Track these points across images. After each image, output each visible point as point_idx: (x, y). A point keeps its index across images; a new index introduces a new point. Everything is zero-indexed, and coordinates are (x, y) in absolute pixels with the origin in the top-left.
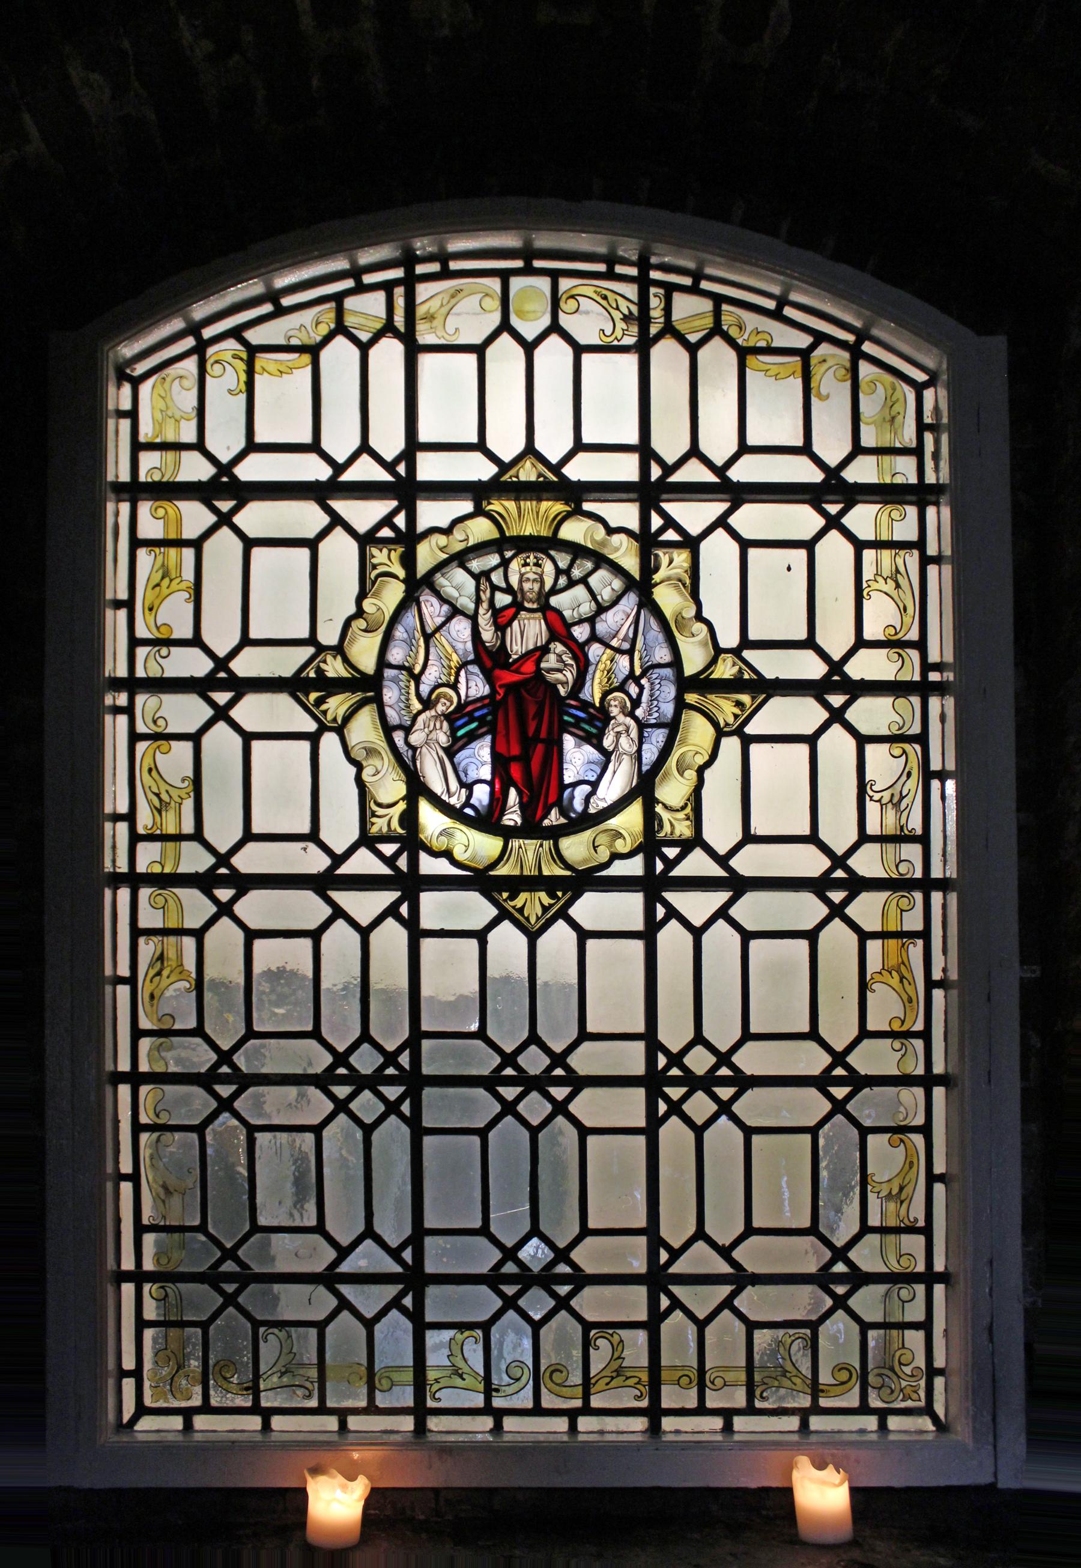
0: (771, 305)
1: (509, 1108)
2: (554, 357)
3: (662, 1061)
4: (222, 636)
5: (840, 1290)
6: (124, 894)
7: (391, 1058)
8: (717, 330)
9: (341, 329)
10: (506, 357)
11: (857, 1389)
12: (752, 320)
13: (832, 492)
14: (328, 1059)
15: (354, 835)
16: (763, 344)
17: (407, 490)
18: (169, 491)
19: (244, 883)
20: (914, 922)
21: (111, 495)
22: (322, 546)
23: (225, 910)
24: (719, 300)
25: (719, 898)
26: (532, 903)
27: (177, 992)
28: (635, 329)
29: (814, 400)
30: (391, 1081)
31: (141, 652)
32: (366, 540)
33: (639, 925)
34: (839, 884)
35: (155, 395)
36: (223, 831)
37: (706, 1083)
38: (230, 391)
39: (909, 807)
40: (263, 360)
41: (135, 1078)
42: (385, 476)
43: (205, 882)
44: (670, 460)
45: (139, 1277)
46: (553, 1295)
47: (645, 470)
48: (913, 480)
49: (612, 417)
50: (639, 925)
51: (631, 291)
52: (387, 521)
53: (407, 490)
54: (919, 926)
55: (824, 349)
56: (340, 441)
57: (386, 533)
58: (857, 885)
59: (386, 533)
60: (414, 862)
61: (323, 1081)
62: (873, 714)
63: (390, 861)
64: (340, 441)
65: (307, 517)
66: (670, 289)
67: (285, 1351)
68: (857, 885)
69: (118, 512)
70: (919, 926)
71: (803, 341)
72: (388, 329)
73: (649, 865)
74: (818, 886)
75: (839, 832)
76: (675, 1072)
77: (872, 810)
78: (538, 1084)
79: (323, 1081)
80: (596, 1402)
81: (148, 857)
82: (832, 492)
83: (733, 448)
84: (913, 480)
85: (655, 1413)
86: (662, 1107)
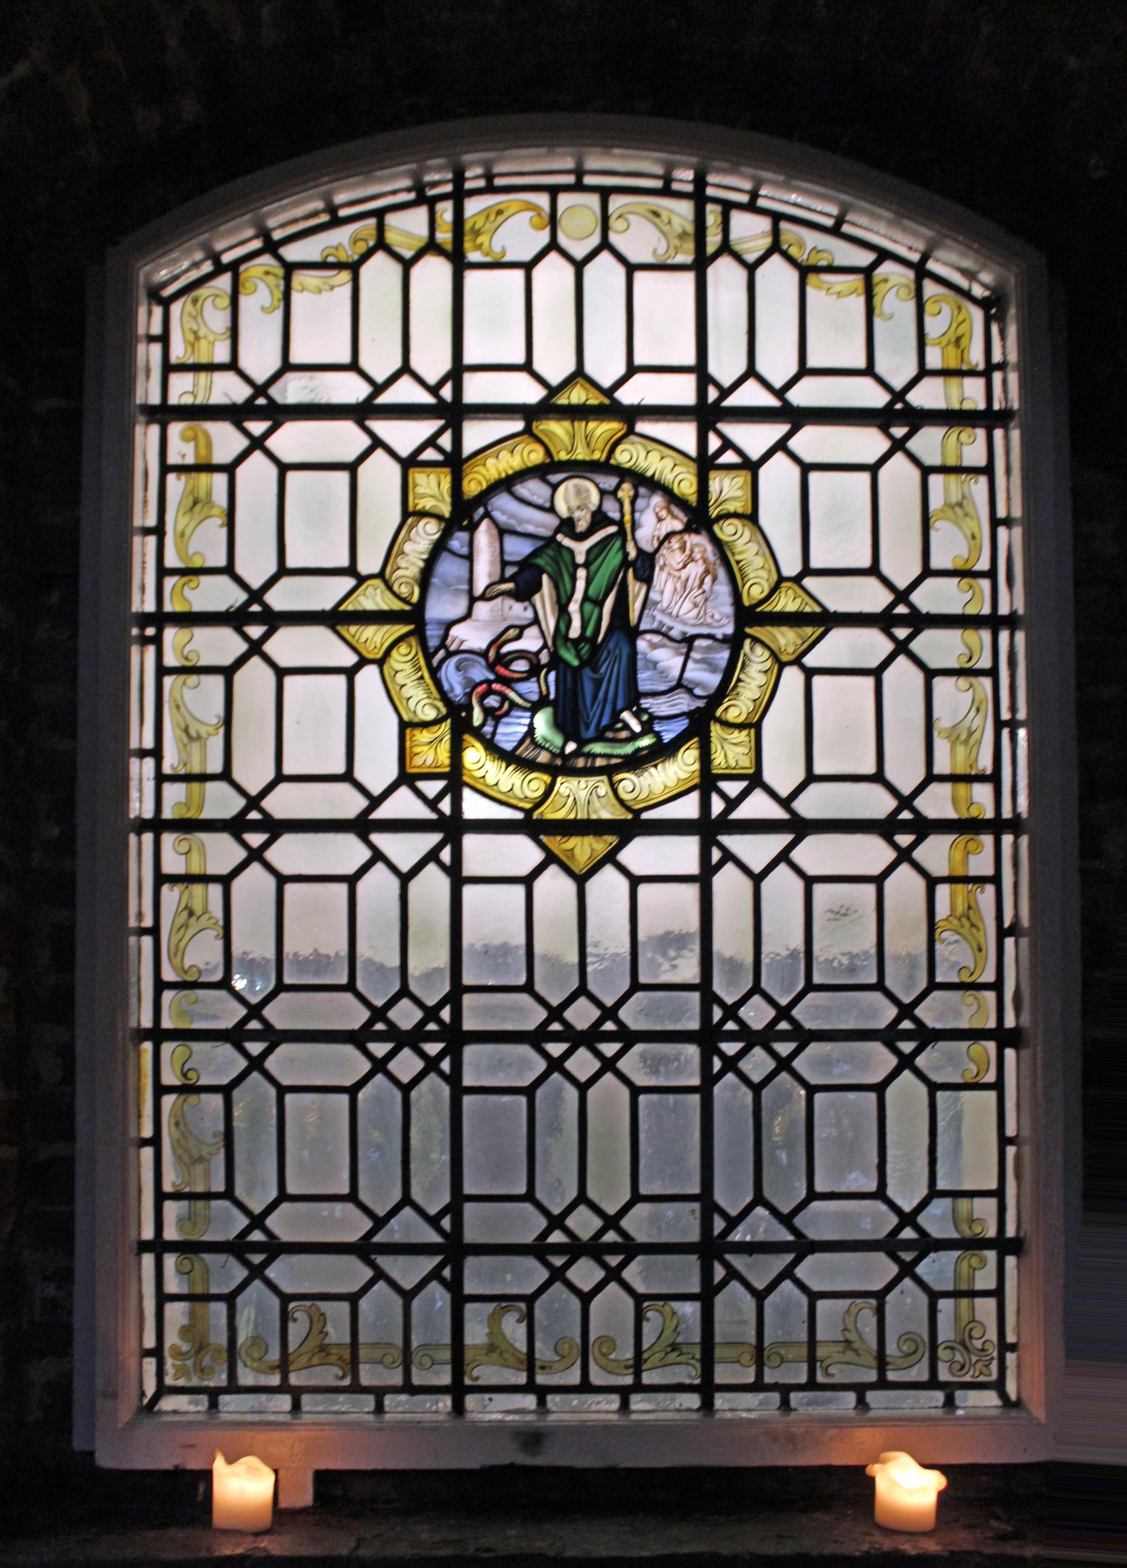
0: (1005, 715)
1: (556, 1065)
2: (604, 275)
3: (717, 1014)
4: (256, 566)
5: (908, 1256)
6: (148, 838)
7: (431, 1013)
8: (776, 247)
9: (382, 244)
10: (554, 276)
11: (926, 1361)
12: (812, 239)
13: (898, 417)
14: (365, 1015)
15: (393, 774)
16: (823, 263)
17: (454, 413)
18: (187, 826)
19: (276, 828)
20: (982, 865)
21: (142, 419)
22: (362, 470)
23: (256, 855)
24: (777, 218)
25: (778, 842)
26: (584, 849)
27: (203, 954)
28: (690, 245)
29: (878, 322)
30: (432, 1037)
31: (169, 582)
32: (409, 463)
33: (694, 869)
34: (905, 826)
35: (186, 318)
36: (253, 772)
37: (764, 1038)
38: (263, 308)
39: (979, 742)
40: (300, 278)
41: (158, 1035)
42: (427, 399)
43: (236, 827)
44: (726, 382)
45: (159, 1247)
46: (604, 1265)
47: (702, 392)
48: (982, 406)
49: (667, 333)
50: (694, 869)
51: (686, 208)
52: (431, 442)
53: (454, 413)
54: (989, 871)
55: (888, 268)
56: (380, 360)
57: (430, 454)
58: (924, 827)
59: (430, 454)
60: (457, 804)
61: (358, 1038)
62: (940, 647)
63: (432, 804)
64: (380, 360)
65: (345, 440)
66: (728, 207)
67: (315, 1331)
68: (924, 827)
69: (147, 437)
70: (989, 871)
71: (865, 258)
72: (431, 247)
73: (705, 805)
74: (886, 828)
75: (905, 772)
76: (730, 1026)
77: (941, 747)
78: (590, 1038)
79: (358, 1038)
80: (647, 1378)
81: (182, 390)
82: (898, 417)
83: (793, 369)
84: (982, 406)
85: (707, 1389)
86: (717, 1064)
